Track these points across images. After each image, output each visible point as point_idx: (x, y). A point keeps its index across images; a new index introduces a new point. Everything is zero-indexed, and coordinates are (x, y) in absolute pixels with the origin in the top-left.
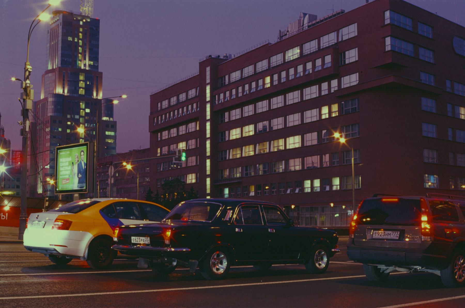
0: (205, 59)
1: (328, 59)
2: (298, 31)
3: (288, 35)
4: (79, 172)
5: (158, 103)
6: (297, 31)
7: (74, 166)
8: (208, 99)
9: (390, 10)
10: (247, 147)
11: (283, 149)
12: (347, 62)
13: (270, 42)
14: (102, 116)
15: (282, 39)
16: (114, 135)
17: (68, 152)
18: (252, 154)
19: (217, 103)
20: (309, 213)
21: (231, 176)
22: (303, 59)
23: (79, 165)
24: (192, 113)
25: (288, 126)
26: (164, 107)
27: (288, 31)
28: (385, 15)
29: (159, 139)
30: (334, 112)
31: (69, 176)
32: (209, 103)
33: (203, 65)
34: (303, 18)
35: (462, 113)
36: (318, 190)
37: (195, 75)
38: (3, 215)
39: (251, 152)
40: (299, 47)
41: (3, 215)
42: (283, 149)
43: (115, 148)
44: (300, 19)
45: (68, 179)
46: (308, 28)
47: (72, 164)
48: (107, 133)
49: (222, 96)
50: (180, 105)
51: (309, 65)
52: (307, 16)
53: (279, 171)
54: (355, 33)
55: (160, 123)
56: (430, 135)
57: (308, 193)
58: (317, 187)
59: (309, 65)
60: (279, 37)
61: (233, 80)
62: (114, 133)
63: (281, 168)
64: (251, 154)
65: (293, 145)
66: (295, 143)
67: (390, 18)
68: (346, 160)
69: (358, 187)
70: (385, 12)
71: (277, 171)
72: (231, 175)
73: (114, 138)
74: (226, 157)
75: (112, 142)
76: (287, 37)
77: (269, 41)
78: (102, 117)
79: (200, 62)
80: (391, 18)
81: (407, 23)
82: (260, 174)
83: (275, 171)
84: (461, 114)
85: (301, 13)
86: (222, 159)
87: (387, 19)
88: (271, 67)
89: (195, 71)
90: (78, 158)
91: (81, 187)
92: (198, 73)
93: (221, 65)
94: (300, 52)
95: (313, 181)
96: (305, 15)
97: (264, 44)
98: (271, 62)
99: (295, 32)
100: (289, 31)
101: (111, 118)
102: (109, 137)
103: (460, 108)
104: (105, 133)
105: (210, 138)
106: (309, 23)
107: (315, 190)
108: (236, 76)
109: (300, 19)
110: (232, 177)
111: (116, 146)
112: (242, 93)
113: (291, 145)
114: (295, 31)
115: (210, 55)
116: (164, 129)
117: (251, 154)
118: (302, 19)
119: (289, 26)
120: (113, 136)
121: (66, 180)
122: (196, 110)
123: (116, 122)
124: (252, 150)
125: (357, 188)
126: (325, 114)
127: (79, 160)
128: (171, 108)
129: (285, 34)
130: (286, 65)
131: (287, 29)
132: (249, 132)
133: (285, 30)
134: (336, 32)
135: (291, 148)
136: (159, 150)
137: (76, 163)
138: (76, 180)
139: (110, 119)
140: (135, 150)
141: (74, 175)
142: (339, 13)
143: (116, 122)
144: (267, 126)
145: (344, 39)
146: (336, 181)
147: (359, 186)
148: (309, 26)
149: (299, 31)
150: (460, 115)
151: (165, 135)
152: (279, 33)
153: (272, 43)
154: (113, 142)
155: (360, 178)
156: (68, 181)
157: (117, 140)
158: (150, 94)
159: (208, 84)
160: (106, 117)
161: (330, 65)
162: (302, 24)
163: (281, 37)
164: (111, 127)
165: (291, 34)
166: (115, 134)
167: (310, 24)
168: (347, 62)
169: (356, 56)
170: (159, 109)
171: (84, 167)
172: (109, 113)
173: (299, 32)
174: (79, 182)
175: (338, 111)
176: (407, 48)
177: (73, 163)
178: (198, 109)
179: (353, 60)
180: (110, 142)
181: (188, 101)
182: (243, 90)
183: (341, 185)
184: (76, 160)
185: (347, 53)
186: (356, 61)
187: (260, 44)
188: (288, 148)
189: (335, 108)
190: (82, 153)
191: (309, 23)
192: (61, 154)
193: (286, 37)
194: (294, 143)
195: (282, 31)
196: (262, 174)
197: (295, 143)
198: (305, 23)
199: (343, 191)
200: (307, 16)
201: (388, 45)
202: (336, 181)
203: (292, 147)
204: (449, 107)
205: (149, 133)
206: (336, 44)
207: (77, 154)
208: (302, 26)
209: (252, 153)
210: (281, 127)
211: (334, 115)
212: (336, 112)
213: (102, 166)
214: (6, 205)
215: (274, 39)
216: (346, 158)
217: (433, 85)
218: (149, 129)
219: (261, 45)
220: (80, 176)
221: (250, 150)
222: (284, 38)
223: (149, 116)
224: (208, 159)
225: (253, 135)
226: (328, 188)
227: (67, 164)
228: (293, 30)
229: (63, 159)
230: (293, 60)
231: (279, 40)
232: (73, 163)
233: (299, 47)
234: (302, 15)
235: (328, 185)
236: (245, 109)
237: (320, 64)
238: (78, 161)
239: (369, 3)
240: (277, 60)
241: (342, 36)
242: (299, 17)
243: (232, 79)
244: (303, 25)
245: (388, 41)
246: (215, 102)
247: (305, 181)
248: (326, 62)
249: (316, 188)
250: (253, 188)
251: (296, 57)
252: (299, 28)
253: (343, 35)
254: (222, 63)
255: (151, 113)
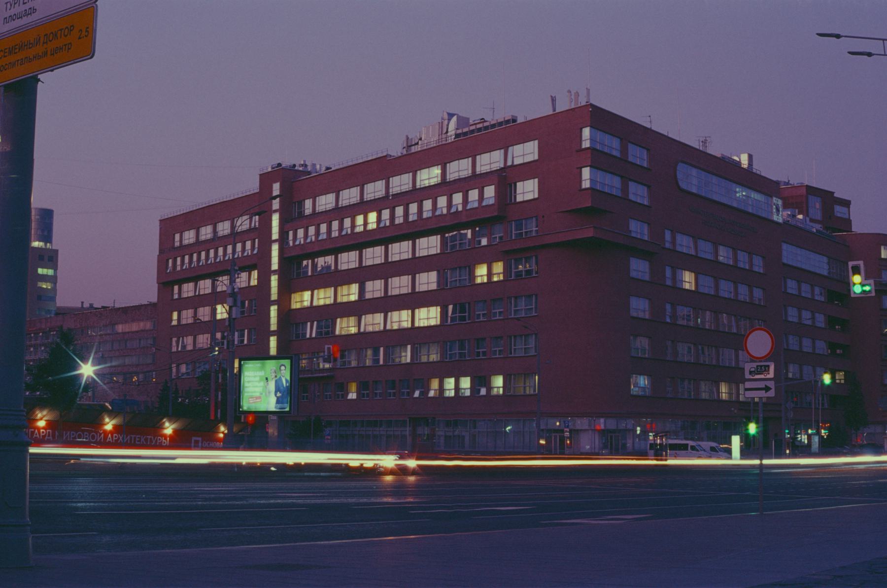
0: (270, 170)
1: (490, 192)
2: (437, 141)
3: (421, 145)
4: (277, 389)
5: (174, 235)
6: (436, 141)
7: (269, 382)
8: (275, 236)
9: (591, 127)
10: (345, 319)
11: (410, 326)
12: (519, 198)
13: (389, 153)
14: (32, 240)
15: (410, 151)
16: (53, 274)
17: (259, 365)
18: (353, 332)
19: (291, 243)
20: (452, 430)
21: (313, 365)
22: (446, 187)
23: (278, 383)
24: (243, 257)
25: (364, 265)
26: (186, 242)
27: (421, 139)
28: (583, 133)
29: (176, 296)
30: (495, 274)
31: (261, 394)
32: (277, 243)
33: (266, 179)
34: (447, 121)
35: (686, 280)
36: (468, 393)
37: (248, 193)
38: (164, 440)
39: (351, 329)
40: (440, 166)
41: (164, 440)
42: (410, 326)
43: (53, 299)
44: (442, 122)
45: (257, 398)
46: (455, 138)
47: (265, 379)
48: (40, 271)
49: (301, 233)
50: (216, 241)
51: (458, 198)
52: (454, 119)
53: (400, 362)
54: (534, 155)
55: (179, 268)
56: (641, 315)
57: (449, 398)
58: (465, 389)
59: (458, 198)
60: (405, 145)
61: (320, 208)
62: (53, 271)
63: (404, 356)
64: (351, 330)
65: (426, 321)
66: (429, 318)
67: (591, 139)
68: (515, 349)
69: (534, 392)
70: (583, 129)
71: (397, 360)
72: (315, 364)
73: (53, 279)
74: (306, 333)
75: (49, 288)
76: (419, 149)
77: (387, 151)
78: (31, 241)
79: (262, 173)
80: (592, 140)
81: (612, 145)
82: (367, 364)
83: (393, 360)
84: (685, 282)
85: (443, 111)
86: (297, 336)
87: (585, 140)
88: (391, 194)
89: (252, 186)
90: (275, 373)
91: (280, 409)
92: (258, 191)
93: (297, 181)
94: (442, 173)
95: (459, 379)
96: (451, 116)
97: (380, 155)
98: (391, 186)
99: (433, 141)
100: (423, 139)
101: (48, 244)
102: (44, 278)
103: (684, 271)
104: (37, 271)
105: (761, 465)
106: (457, 129)
107: (462, 394)
108: (326, 202)
109: (442, 122)
110: (316, 367)
111: (56, 295)
112: (339, 232)
113: (421, 321)
114: (432, 140)
115: (281, 163)
116: (187, 280)
117: (351, 330)
118: (446, 122)
119: (423, 130)
120: (52, 276)
121: (255, 399)
122: (251, 253)
123: (56, 251)
124: (354, 325)
125: (532, 392)
126: (482, 276)
127: (277, 376)
128: (200, 245)
129: (416, 142)
130: (418, 194)
131: (420, 135)
132: (349, 295)
133: (416, 136)
134: (502, 151)
135: (422, 325)
136: (175, 315)
137: (273, 379)
138: (273, 400)
139: (46, 245)
140: (108, 307)
141: (269, 393)
142: (508, 122)
143: (56, 251)
144: (331, 264)
145: (515, 163)
146: (498, 382)
147: (535, 390)
148: (457, 136)
149: (440, 140)
150: (684, 283)
151: (188, 290)
152: (405, 139)
153: (392, 154)
154: (51, 287)
155: (537, 377)
156: (258, 400)
157: (57, 284)
158: (159, 218)
159: (275, 211)
160: (40, 241)
161: (492, 201)
162: (445, 131)
163: (409, 147)
164: (49, 260)
165: (426, 144)
166: (54, 273)
167: (459, 131)
168: (519, 198)
169: (535, 189)
170: (177, 244)
171: (286, 384)
172: (46, 233)
173: (440, 143)
174: (278, 402)
175: (504, 273)
176: (612, 183)
177: (267, 379)
178: (255, 252)
179: (529, 197)
180: (44, 286)
181: (235, 237)
182: (341, 228)
183: (505, 387)
184: (272, 376)
185: (519, 185)
186: (534, 199)
187: (372, 155)
188: (417, 325)
189: (498, 267)
190: (283, 368)
191: (457, 129)
192: (246, 366)
193: (418, 148)
194: (428, 318)
195: (410, 137)
196: (371, 365)
197: (429, 318)
198: (449, 130)
199: (508, 396)
200: (454, 119)
201: (585, 180)
202: (498, 382)
203: (424, 323)
204: (668, 272)
205: (157, 285)
206: (502, 169)
207: (274, 368)
208: (445, 134)
209: (353, 330)
210: (353, 266)
211: (495, 279)
212: (499, 274)
213: (41, 334)
214: (108, 423)
215: (396, 150)
216: (515, 346)
217: (646, 239)
218: (158, 278)
219: (374, 157)
220: (279, 394)
221: (350, 326)
222: (414, 149)
223: (158, 256)
224: (274, 335)
225: (355, 301)
226: (483, 391)
227: (258, 379)
228: (430, 138)
229: (250, 372)
230: (430, 187)
231: (405, 152)
232: (267, 379)
233: (440, 166)
234: (446, 116)
235: (485, 386)
236: (342, 257)
237: (477, 198)
238: (276, 376)
239: (556, 112)
240: (401, 183)
241: (513, 158)
242: (441, 118)
243: (319, 206)
244: (447, 132)
245: (586, 173)
246: (288, 243)
247: (445, 379)
248: (485, 197)
249: (463, 391)
250: (353, 387)
251: (433, 182)
252: (440, 136)
253: (515, 156)
254: (300, 179)
255: (161, 251)
